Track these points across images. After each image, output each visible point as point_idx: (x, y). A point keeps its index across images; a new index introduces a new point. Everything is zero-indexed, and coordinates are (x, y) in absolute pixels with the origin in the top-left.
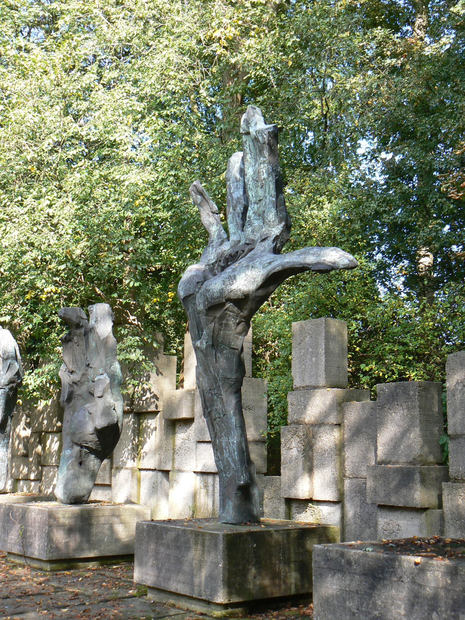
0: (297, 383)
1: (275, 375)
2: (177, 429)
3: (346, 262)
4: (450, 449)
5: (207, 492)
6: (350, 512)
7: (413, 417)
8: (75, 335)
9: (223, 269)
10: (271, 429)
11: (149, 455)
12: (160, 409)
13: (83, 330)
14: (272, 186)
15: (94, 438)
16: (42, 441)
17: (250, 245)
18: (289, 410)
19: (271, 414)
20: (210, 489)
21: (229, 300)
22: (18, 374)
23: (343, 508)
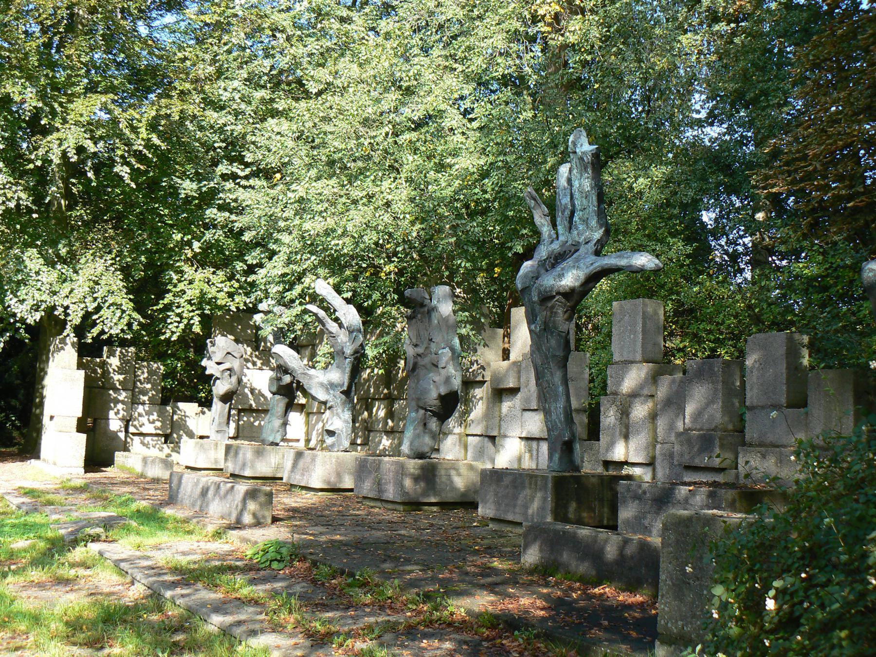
0: (616, 357)
1: (597, 349)
2: (504, 398)
3: (653, 265)
4: (747, 419)
5: (531, 456)
6: (660, 474)
7: (716, 390)
8: (419, 313)
9: (553, 266)
10: (592, 399)
11: (475, 423)
12: (488, 378)
13: (426, 309)
14: (595, 198)
15: (437, 403)
16: (369, 408)
17: (576, 247)
18: (609, 382)
19: (592, 385)
20: (535, 453)
21: (558, 293)
22: (361, 345)
23: (654, 470)
